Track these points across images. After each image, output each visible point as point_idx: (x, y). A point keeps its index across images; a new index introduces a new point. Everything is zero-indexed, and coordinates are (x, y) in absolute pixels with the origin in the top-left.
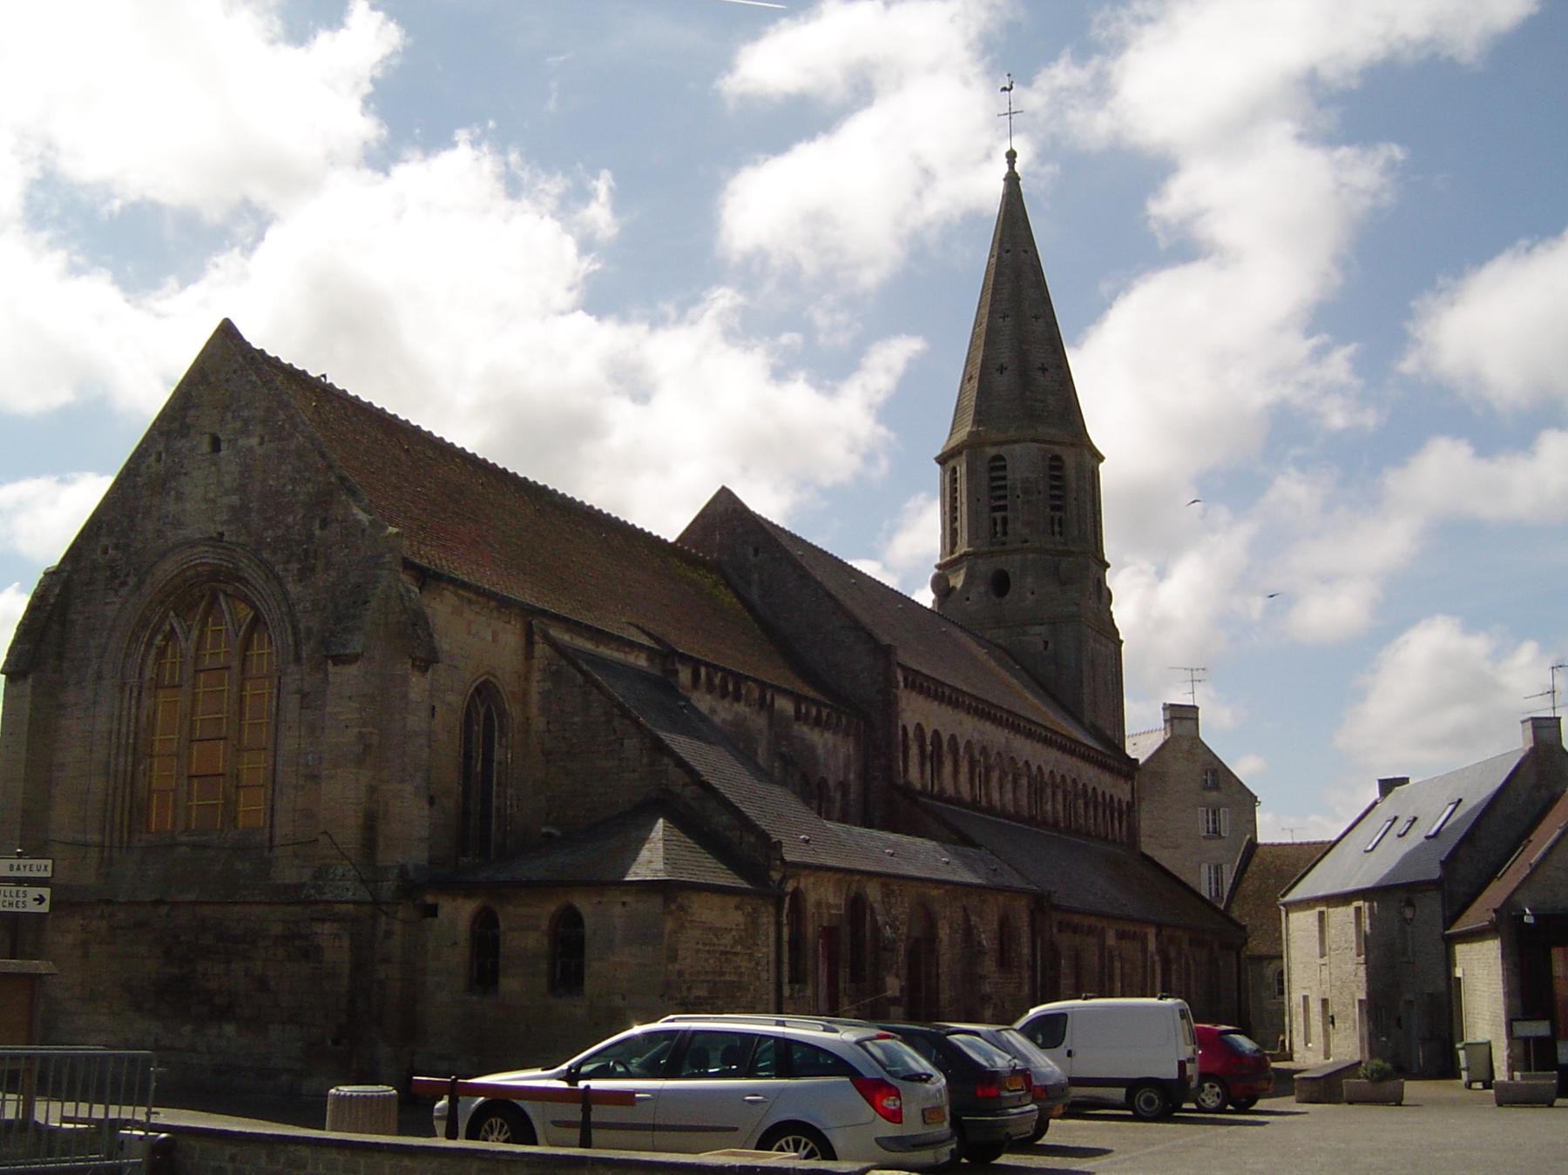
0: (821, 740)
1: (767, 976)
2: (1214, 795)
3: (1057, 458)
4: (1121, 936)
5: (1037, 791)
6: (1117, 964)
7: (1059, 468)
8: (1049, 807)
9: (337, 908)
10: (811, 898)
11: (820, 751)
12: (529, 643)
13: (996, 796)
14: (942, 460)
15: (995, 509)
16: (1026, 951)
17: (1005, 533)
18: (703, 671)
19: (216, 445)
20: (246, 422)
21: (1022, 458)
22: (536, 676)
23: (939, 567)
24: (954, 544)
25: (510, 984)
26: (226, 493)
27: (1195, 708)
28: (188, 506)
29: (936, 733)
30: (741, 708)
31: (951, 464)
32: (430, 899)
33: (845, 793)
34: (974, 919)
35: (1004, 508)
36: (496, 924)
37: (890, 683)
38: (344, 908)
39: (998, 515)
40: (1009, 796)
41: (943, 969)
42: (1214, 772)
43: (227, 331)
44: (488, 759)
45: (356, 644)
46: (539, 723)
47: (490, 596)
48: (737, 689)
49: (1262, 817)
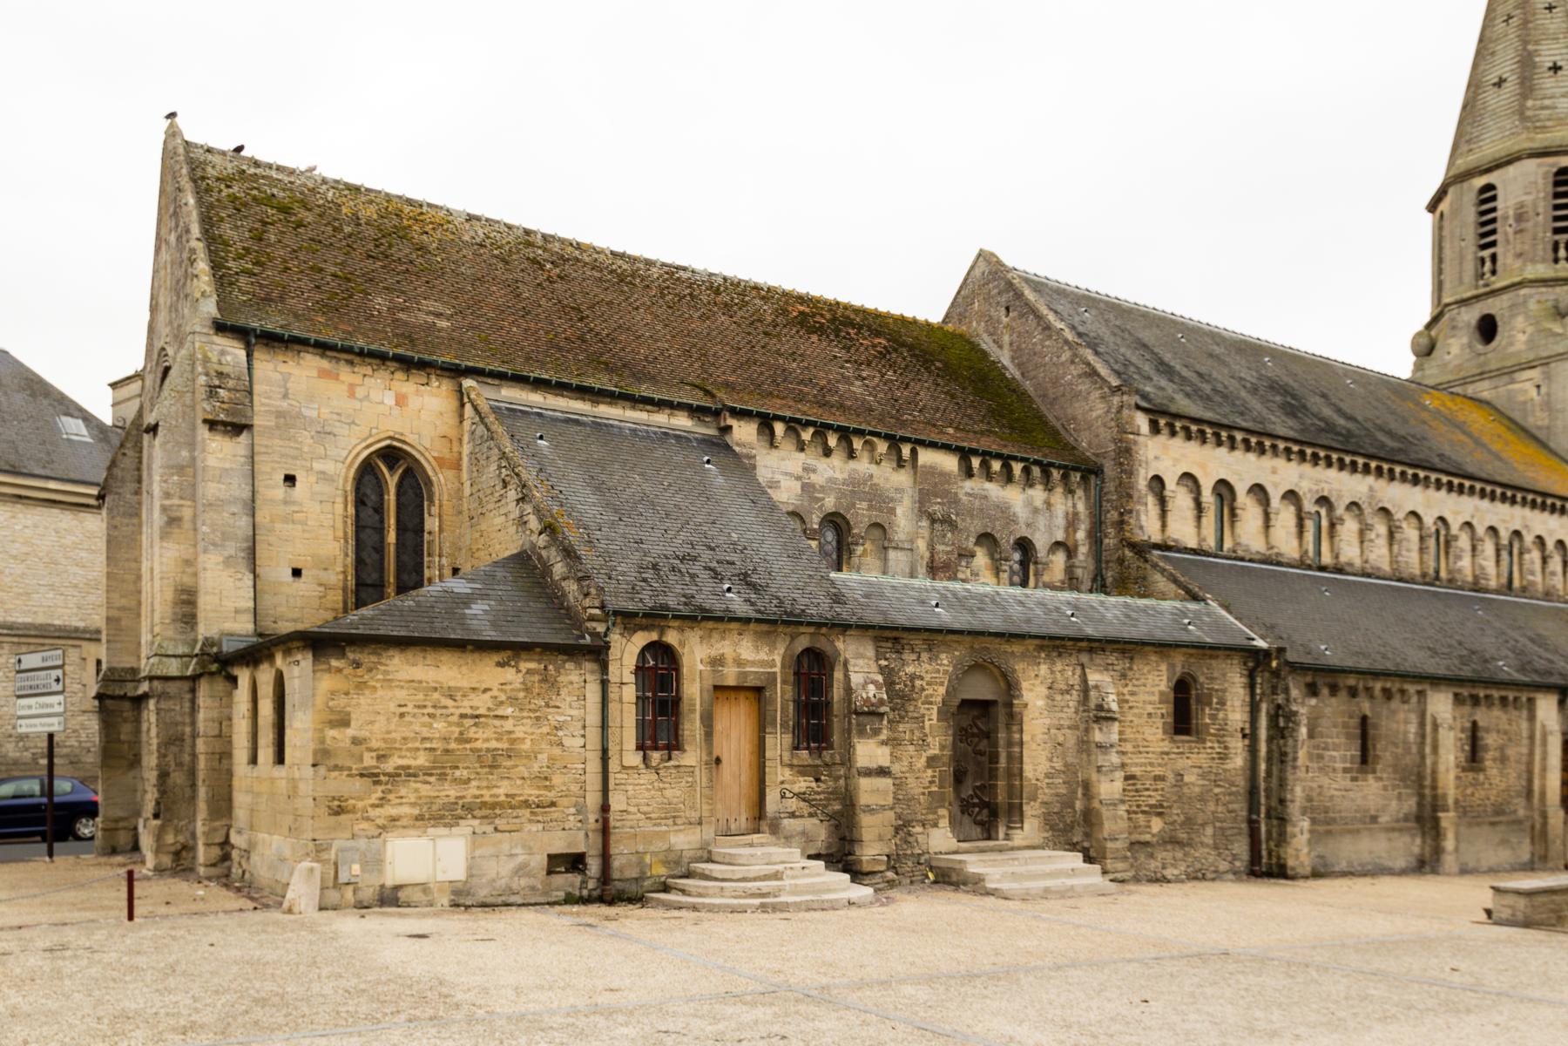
14: (1432, 207)
15: (1484, 247)
17: (1494, 272)
35: (1493, 244)
37: (1124, 430)
39: (1486, 253)
47: (372, 355)
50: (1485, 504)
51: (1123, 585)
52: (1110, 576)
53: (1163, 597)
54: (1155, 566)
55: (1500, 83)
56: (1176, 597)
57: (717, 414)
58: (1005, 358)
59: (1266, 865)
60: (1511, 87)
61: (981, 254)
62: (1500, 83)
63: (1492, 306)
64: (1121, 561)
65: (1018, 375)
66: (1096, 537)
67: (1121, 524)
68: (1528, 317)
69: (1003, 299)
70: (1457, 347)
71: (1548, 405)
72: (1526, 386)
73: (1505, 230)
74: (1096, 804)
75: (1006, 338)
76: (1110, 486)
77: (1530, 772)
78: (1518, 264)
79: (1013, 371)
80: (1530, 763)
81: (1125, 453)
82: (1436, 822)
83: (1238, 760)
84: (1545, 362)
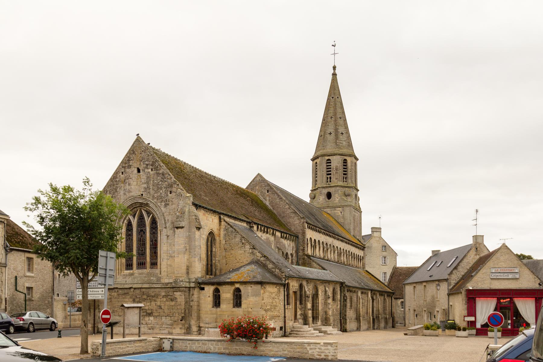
0: (286, 243)
1: (282, 303)
2: (384, 254)
3: (345, 160)
4: (362, 293)
5: (339, 255)
6: (361, 300)
7: (346, 163)
8: (342, 258)
9: (181, 289)
10: (291, 284)
11: (286, 246)
12: (220, 221)
13: (329, 256)
14: (313, 160)
15: (328, 174)
16: (339, 297)
17: (330, 181)
18: (259, 226)
19: (139, 171)
20: (147, 165)
21: (336, 161)
22: (222, 230)
23: (312, 191)
24: (316, 184)
25: (223, 306)
26: (143, 183)
27: (380, 228)
28: (132, 187)
29: (315, 240)
30: (268, 235)
31: (315, 161)
32: (202, 286)
33: (292, 256)
34: (327, 289)
35: (330, 174)
36: (219, 292)
37: (304, 228)
38: (182, 289)
39: (329, 176)
40: (332, 256)
41: (320, 301)
42: (385, 246)
43: (139, 140)
44: (211, 251)
45: (182, 224)
46: (223, 242)
47: (211, 210)
48: (267, 230)
49: (398, 259)
50: (317, 234)
51: (304, 264)
52: (300, 262)
53: (316, 268)
54: (313, 261)
55: (330, 134)
56: (319, 269)
57: (250, 223)
58: (267, 203)
59: (95, 300)
60: (333, 135)
61: (259, 174)
62: (330, 134)
63: (331, 190)
64: (304, 259)
65: (272, 208)
66: (297, 252)
67: (303, 250)
68: (339, 195)
69: (267, 188)
70: (321, 198)
71: (343, 217)
72: (338, 211)
73: (333, 172)
74: (328, 316)
75: (268, 198)
76: (301, 241)
77: (367, 308)
78: (336, 181)
79: (270, 207)
80: (367, 307)
81: (304, 233)
82: (360, 319)
83: (339, 307)
84: (343, 207)
